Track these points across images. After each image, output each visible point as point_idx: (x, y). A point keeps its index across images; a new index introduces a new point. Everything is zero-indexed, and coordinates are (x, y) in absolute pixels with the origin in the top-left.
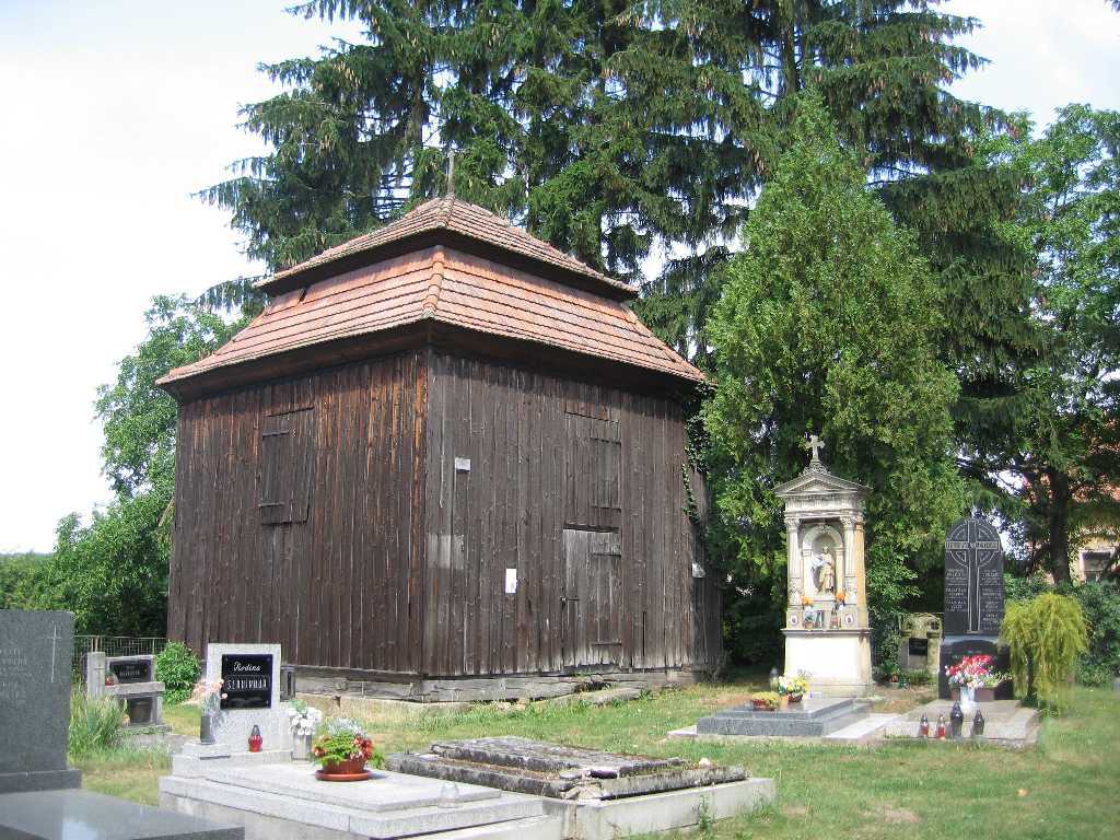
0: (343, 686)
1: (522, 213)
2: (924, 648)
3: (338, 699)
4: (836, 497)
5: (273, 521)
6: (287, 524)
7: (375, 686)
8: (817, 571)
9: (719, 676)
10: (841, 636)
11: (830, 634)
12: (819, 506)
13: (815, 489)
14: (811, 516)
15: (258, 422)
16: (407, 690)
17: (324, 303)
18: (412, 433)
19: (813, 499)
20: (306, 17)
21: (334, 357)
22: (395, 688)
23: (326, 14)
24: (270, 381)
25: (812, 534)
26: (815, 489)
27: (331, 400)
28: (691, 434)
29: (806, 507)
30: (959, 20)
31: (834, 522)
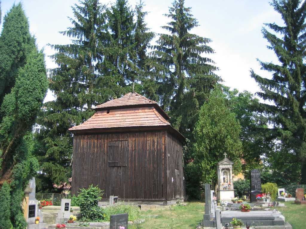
0: (141, 203)
1: (274, 114)
2: (66, 209)
3: (140, 206)
4: (229, 164)
5: (113, 165)
6: (117, 167)
7: (151, 203)
8: (224, 178)
9: (187, 201)
10: (230, 191)
11: (229, 190)
12: (226, 166)
13: (225, 163)
14: (224, 168)
15: (105, 143)
16: (162, 203)
17: (118, 115)
18: (161, 148)
19: (225, 165)
20: (64, 35)
21: (137, 130)
22: (158, 203)
23: (69, 35)
24: (91, 134)
25: (223, 171)
26: (225, 163)
27: (134, 139)
28: (183, 149)
29: (224, 166)
30: (215, 67)
31: (228, 169)
